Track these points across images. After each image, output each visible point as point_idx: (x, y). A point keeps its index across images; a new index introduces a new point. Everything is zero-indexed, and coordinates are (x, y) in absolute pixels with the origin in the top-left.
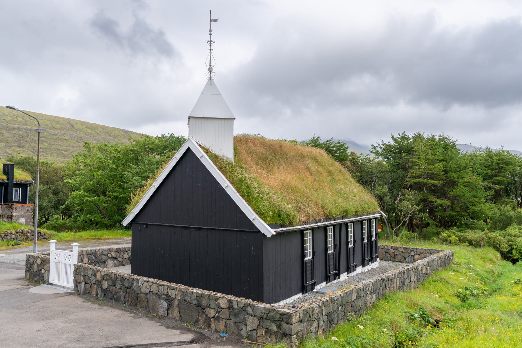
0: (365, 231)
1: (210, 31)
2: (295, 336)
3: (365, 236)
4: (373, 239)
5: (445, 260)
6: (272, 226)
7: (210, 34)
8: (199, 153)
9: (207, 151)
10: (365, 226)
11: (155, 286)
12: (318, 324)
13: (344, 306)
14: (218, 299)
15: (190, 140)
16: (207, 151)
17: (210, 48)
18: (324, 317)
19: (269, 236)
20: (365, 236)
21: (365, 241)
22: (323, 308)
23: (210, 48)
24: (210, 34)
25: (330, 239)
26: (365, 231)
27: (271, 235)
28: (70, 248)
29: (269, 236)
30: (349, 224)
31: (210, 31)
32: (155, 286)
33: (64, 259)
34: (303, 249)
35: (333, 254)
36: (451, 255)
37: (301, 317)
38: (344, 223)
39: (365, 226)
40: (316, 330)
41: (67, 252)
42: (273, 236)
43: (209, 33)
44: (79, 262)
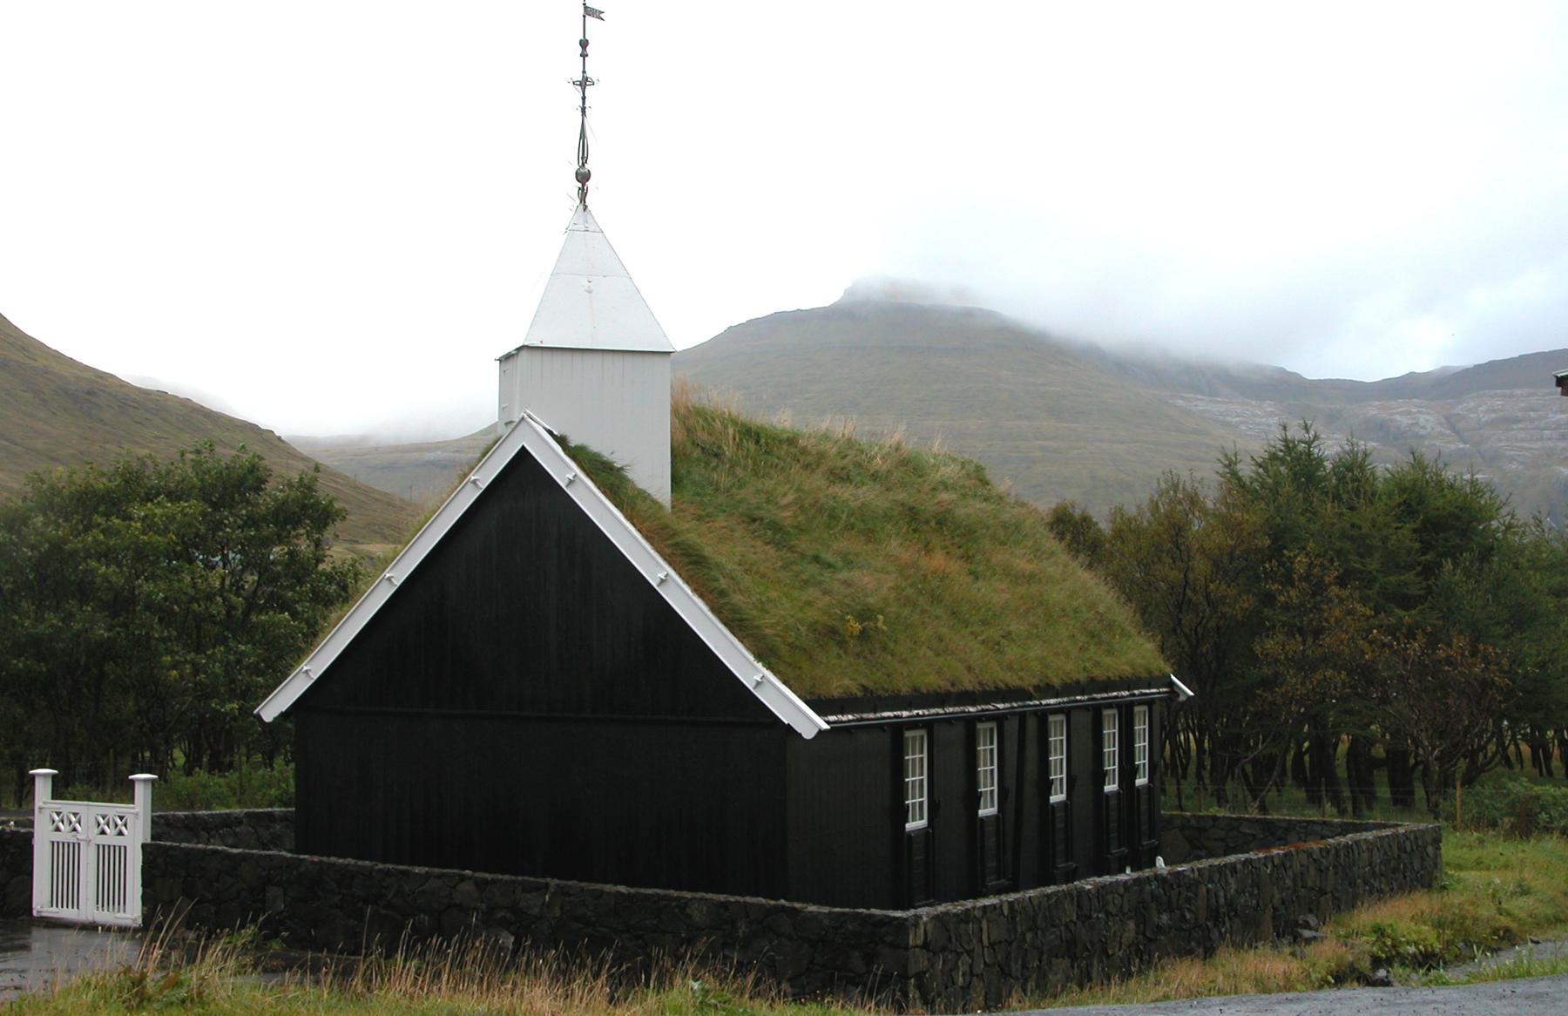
0: (1111, 749)
1: (584, 44)
2: (913, 981)
3: (1112, 767)
4: (1141, 781)
5: (1404, 856)
6: (820, 705)
7: (584, 55)
8: (562, 470)
9: (578, 454)
10: (1111, 731)
11: (466, 887)
12: (971, 966)
13: (1039, 933)
14: (686, 903)
15: (528, 423)
16: (578, 454)
17: (584, 103)
18: (986, 949)
19: (808, 734)
20: (1112, 767)
21: (1110, 788)
22: (984, 925)
23: (584, 103)
24: (584, 55)
25: (985, 765)
26: (1111, 749)
27: (816, 731)
28: (125, 793)
29: (808, 734)
30: (1051, 718)
31: (584, 44)
32: (466, 887)
33: (97, 831)
34: (900, 790)
35: (997, 819)
36: (1429, 839)
37: (930, 935)
38: (1035, 713)
39: (1111, 731)
40: (964, 979)
41: (113, 809)
42: (821, 732)
43: (580, 49)
44: (153, 838)
